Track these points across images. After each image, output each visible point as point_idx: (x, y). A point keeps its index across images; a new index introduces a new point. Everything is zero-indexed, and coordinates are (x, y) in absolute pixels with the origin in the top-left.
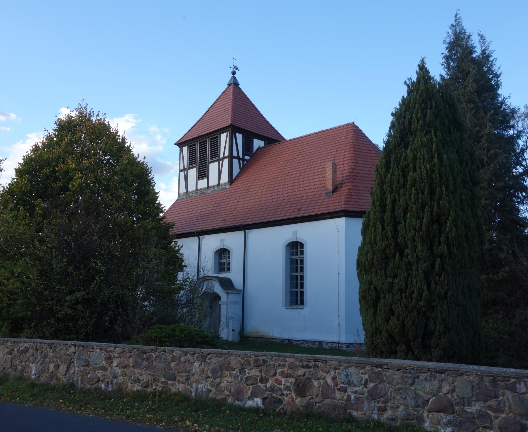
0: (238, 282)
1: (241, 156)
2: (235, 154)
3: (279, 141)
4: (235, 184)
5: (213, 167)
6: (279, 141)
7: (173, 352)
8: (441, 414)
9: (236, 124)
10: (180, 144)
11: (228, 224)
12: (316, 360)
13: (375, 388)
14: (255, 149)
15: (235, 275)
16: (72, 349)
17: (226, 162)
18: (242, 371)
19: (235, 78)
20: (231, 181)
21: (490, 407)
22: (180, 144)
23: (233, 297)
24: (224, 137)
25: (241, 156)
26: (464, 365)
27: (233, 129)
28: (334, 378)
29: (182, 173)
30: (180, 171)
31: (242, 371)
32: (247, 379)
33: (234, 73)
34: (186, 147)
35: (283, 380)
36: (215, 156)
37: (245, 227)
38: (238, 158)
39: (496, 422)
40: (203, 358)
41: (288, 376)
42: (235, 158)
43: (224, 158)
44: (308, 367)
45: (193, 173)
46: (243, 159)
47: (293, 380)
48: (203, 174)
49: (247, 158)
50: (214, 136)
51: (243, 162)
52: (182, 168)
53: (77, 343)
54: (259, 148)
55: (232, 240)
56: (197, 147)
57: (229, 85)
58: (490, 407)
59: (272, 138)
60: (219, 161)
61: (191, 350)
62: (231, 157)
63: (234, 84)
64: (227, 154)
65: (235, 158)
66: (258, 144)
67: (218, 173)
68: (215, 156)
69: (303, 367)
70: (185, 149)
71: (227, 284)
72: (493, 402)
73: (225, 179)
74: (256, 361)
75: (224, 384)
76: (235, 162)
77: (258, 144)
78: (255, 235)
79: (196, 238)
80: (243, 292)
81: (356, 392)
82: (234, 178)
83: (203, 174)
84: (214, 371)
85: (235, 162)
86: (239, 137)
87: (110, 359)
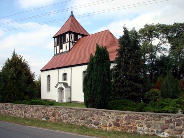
0: (69, 85)
1: (73, 41)
2: (71, 41)
3: (87, 35)
4: (57, 56)
5: (64, 45)
6: (87, 35)
7: (26, 106)
8: (83, 120)
9: (71, 31)
10: (54, 37)
11: (68, 65)
12: (57, 108)
13: (69, 114)
14: (78, 39)
15: (68, 82)
16: (4, 105)
17: (68, 43)
18: (41, 111)
19: (72, 14)
20: (70, 50)
21: (92, 118)
22: (54, 37)
23: (68, 89)
24: (67, 35)
25: (73, 41)
26: (28, 106)
27: (70, 32)
28: (61, 112)
29: (55, 47)
30: (55, 46)
31: (41, 111)
32: (43, 112)
33: (72, 12)
34: (68, 34)
35: (50, 113)
36: (65, 41)
37: (58, 68)
38: (72, 42)
39: (93, 122)
40: (32, 107)
41: (51, 112)
42: (71, 42)
43: (68, 42)
44: (55, 109)
45: (58, 47)
46: (74, 42)
47: (52, 113)
48: (61, 48)
49: (75, 42)
50: (64, 34)
51: (74, 43)
52: (55, 45)
53: (5, 103)
54: (80, 38)
55: (67, 70)
56: (60, 38)
57: (71, 16)
58: (92, 118)
59: (84, 35)
60: (66, 43)
61: (30, 105)
62: (70, 42)
63: (72, 16)
64: (68, 41)
65: (71, 42)
66: (79, 37)
67: (66, 47)
68: (65, 41)
69: (54, 109)
70: (56, 39)
71: (66, 85)
72: (93, 117)
73: (68, 49)
74: (44, 108)
75: (37, 114)
76: (71, 43)
77: (79, 37)
78: (73, 68)
79: (57, 70)
80: (70, 87)
81: (65, 115)
82: (71, 48)
83: (61, 48)
84: (35, 111)
85: (71, 43)
86: (73, 35)
87: (12, 108)
